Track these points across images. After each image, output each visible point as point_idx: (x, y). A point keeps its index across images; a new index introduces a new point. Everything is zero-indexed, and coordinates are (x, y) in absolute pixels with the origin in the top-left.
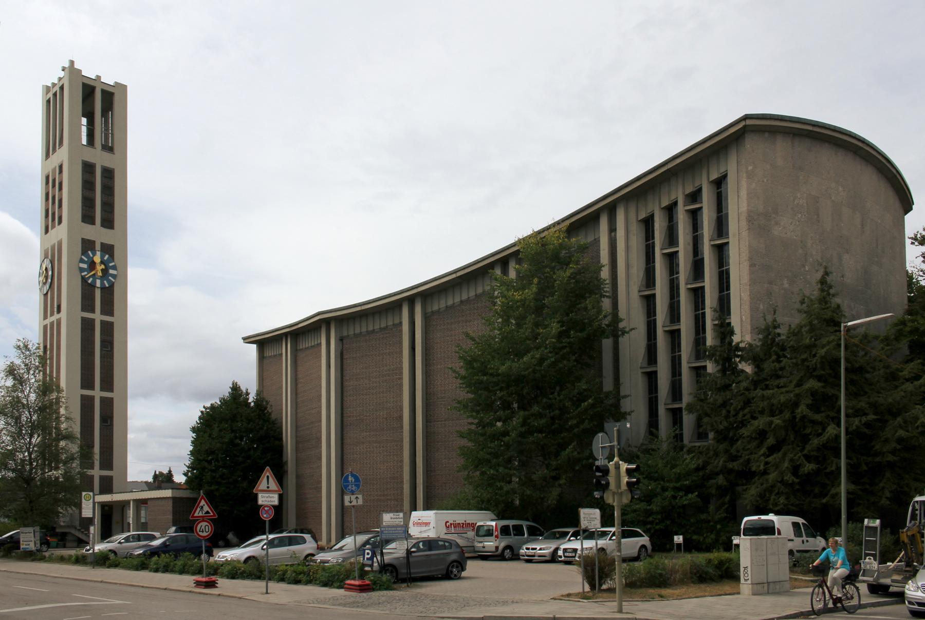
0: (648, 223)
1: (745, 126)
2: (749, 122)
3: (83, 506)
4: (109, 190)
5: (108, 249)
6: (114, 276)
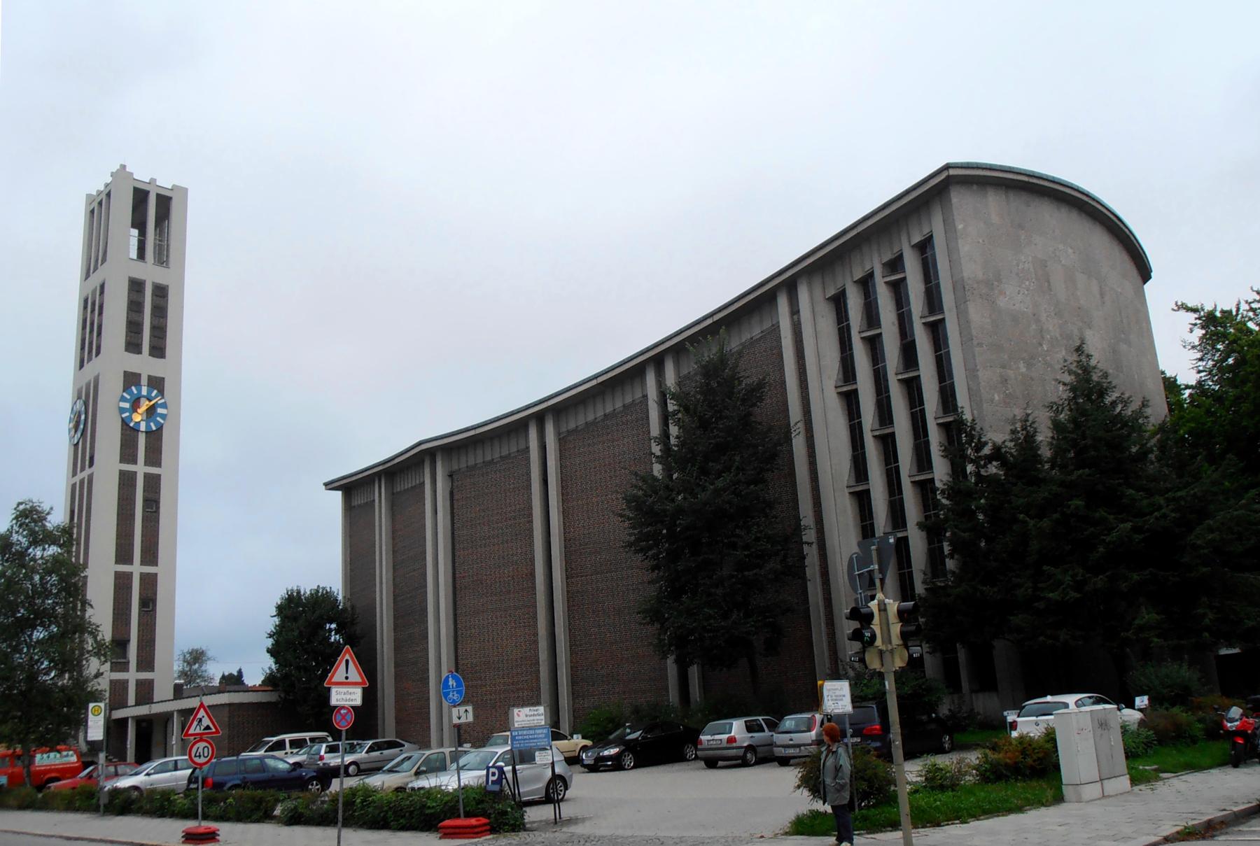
0: (839, 302)
1: (948, 177)
2: (952, 172)
3: (90, 723)
4: (160, 311)
5: (157, 384)
6: (164, 417)
